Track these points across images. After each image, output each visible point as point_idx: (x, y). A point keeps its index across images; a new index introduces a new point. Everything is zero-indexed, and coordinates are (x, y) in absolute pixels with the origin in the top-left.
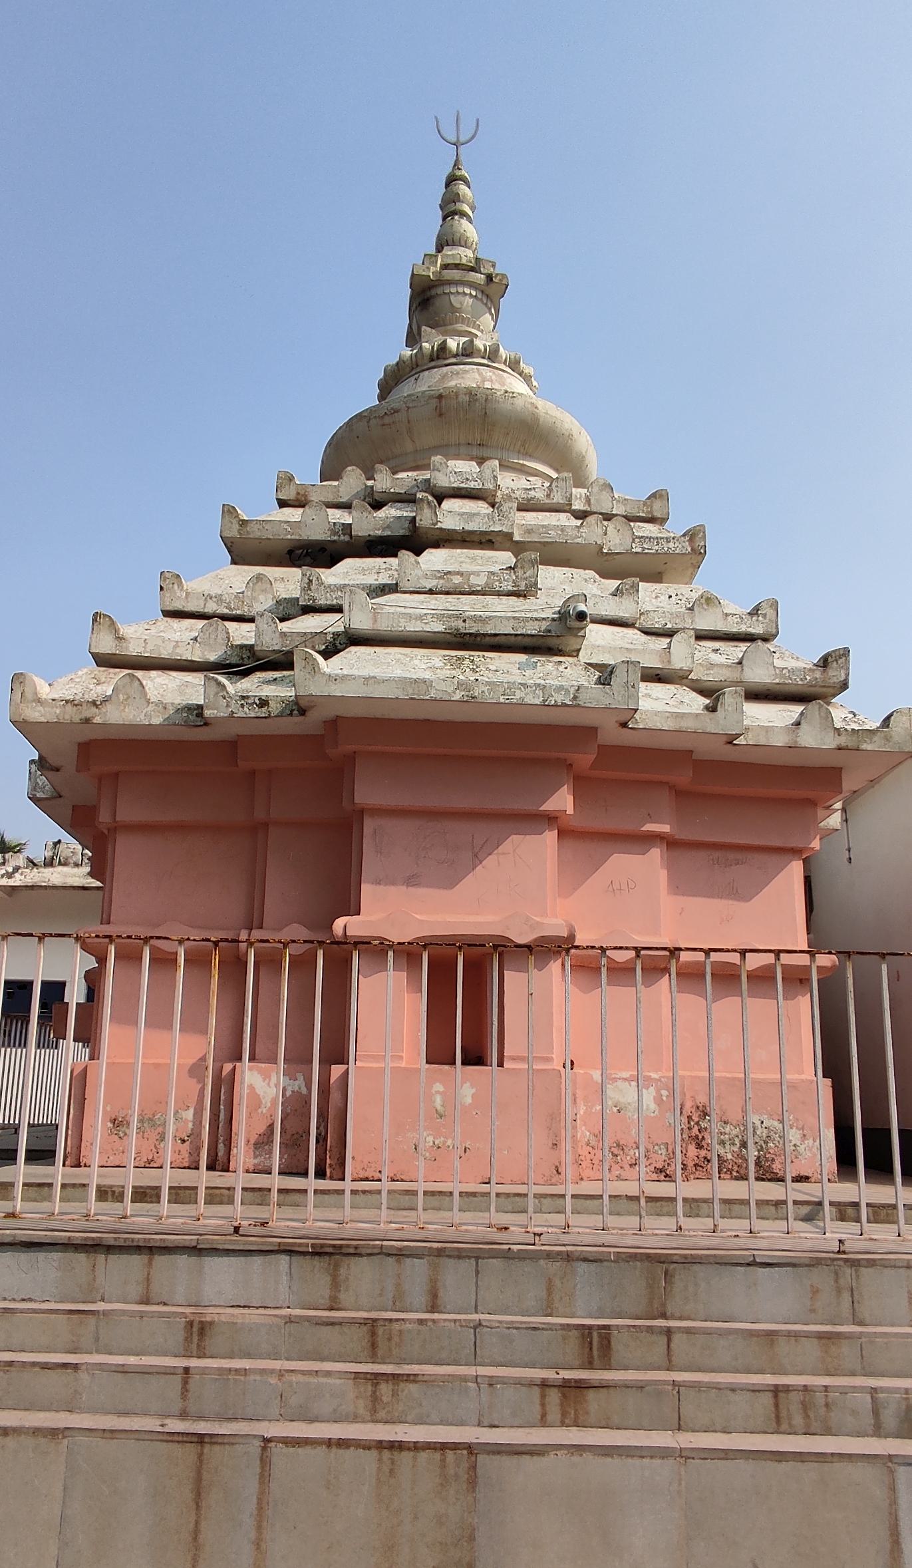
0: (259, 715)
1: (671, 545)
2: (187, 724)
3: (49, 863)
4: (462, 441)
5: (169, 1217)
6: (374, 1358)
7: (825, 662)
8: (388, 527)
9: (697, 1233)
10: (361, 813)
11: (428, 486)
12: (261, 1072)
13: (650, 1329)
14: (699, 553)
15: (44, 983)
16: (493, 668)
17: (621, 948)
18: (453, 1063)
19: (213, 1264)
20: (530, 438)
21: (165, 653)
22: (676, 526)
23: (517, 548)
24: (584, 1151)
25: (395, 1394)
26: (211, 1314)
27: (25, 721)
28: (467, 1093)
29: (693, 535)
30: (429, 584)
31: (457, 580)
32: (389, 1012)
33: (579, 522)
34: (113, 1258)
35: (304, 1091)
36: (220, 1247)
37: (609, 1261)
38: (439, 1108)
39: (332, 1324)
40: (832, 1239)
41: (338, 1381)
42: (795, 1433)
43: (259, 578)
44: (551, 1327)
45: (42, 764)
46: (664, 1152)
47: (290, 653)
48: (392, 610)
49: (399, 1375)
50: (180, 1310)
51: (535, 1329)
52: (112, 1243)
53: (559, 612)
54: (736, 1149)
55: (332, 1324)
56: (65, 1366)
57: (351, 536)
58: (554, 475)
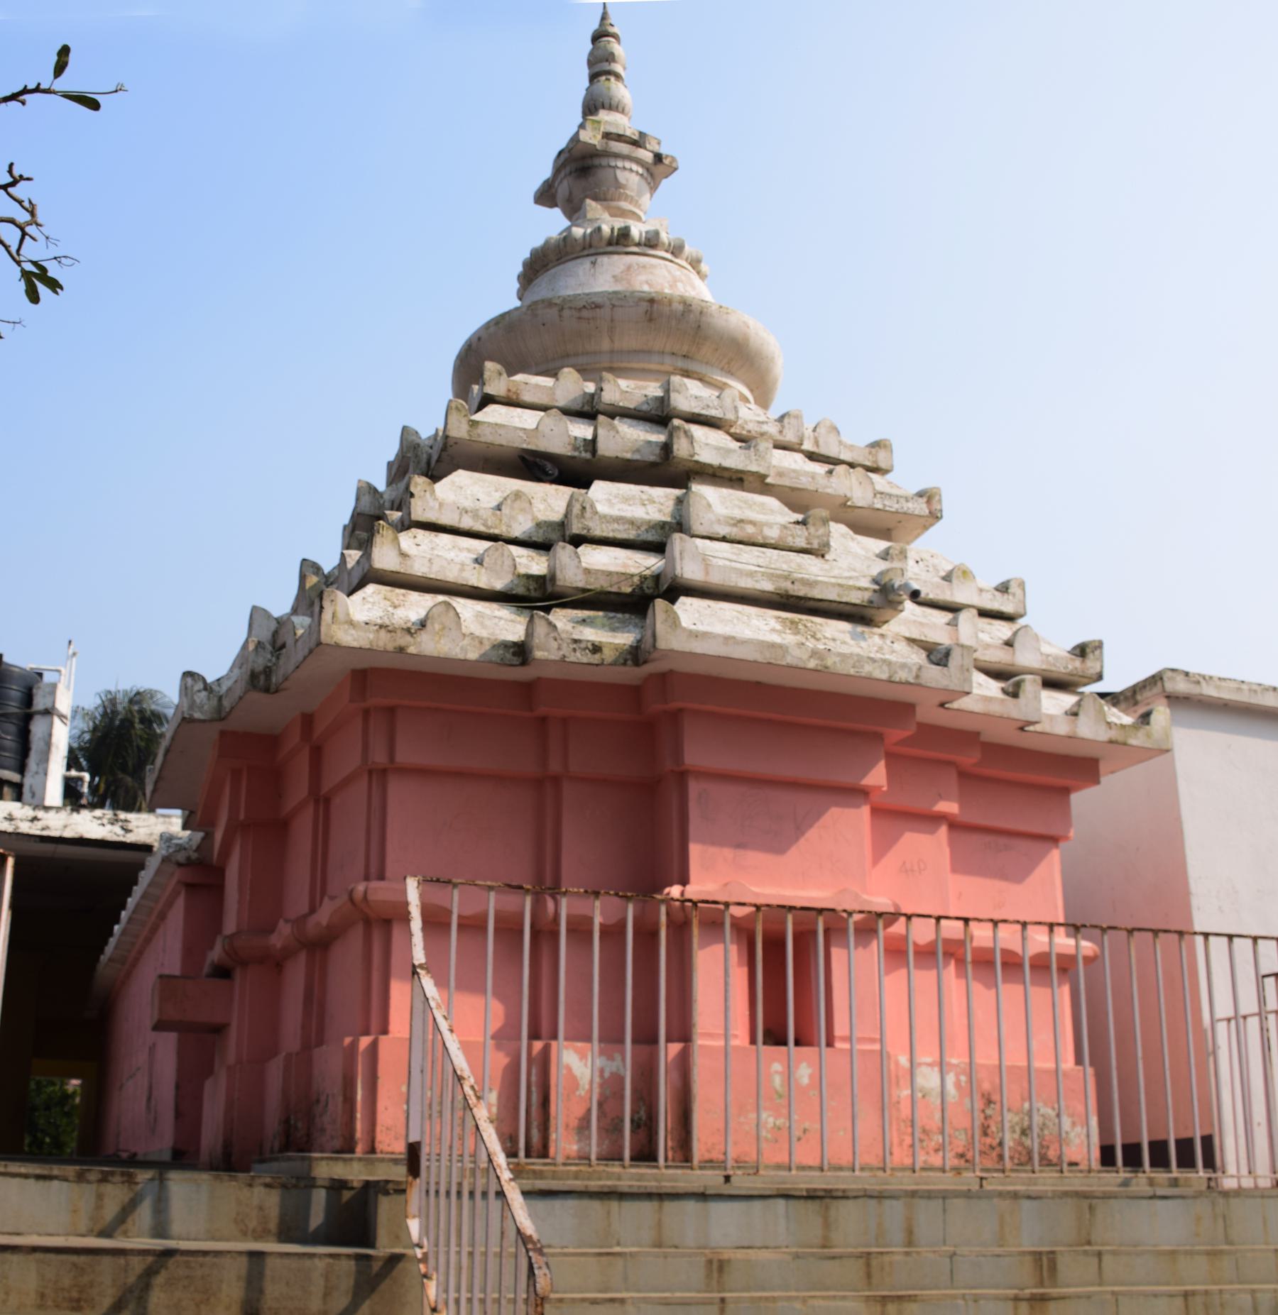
2: (503, 663)
4: (668, 349)
7: (1082, 651)
8: (638, 451)
12: (577, 1051)
18: (785, 1043)
19: (717, 1207)
26: (726, 1255)
28: (804, 1073)
29: (928, 495)
30: (723, 530)
31: (750, 530)
32: (719, 983)
37: (1047, 1198)
43: (518, 495)
46: (963, 1137)
53: (875, 581)
54: (1016, 1136)
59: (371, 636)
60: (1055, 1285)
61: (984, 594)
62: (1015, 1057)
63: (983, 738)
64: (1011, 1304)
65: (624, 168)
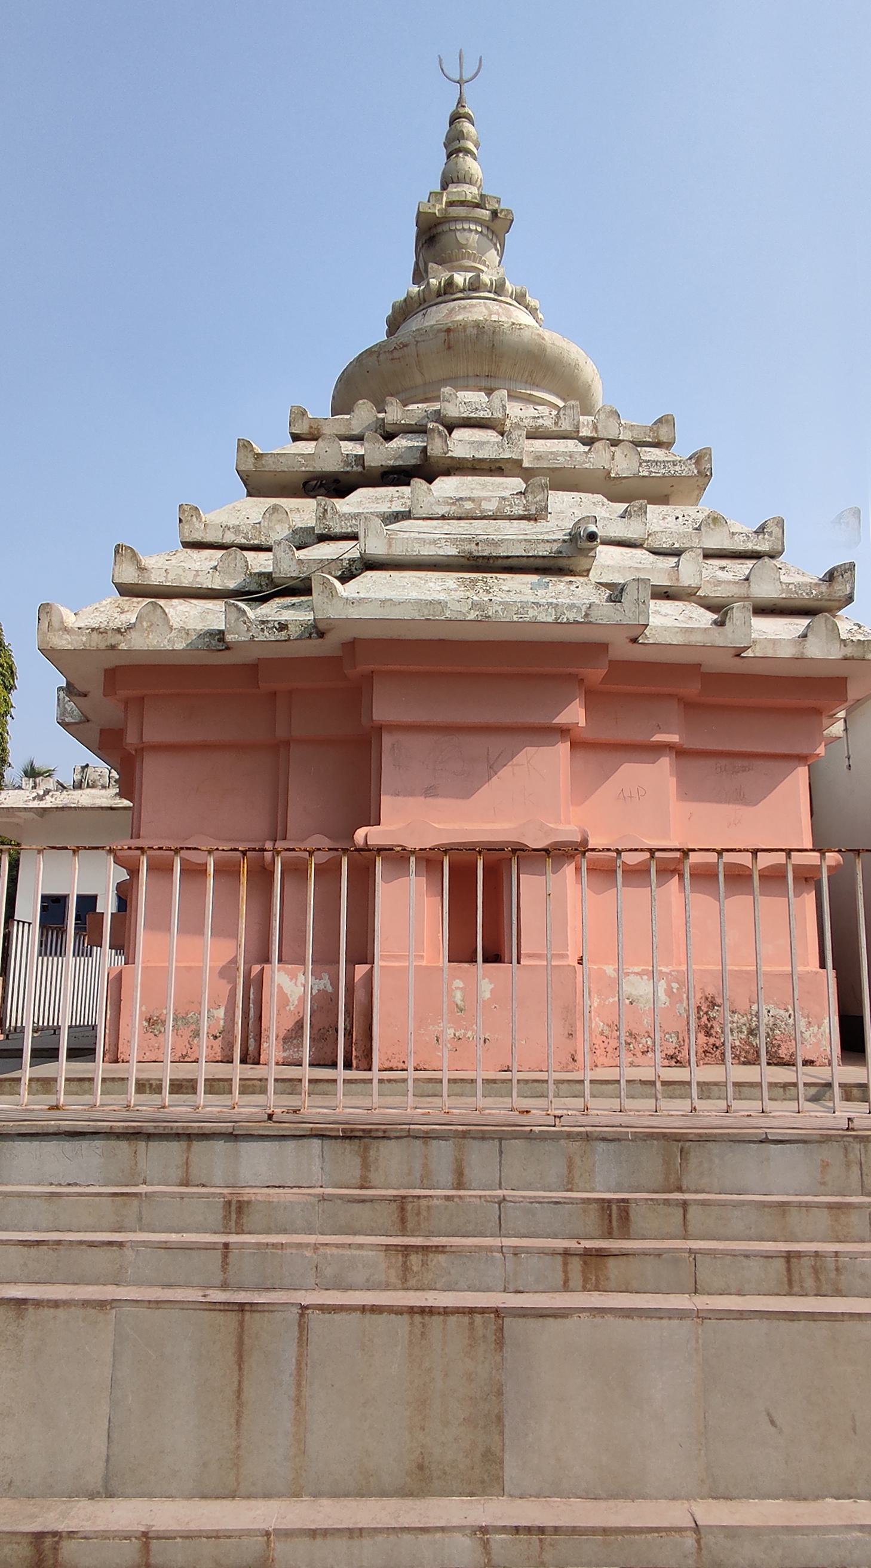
0: (278, 638)
1: (677, 468)
3: (78, 786)
5: (206, 1107)
6: (404, 1232)
7: (831, 577)
8: (400, 457)
9: (710, 1113)
10: (379, 729)
11: (438, 416)
12: (287, 972)
13: (667, 1202)
14: (705, 476)
15: (79, 897)
16: (506, 588)
17: (636, 850)
18: (473, 960)
20: (538, 369)
21: (187, 581)
22: (682, 450)
23: (527, 474)
24: (598, 1041)
25: (424, 1263)
26: (247, 1194)
27: (53, 649)
28: (486, 989)
29: (700, 458)
31: (469, 505)
32: (410, 916)
33: (587, 448)
34: (153, 1145)
35: (330, 989)
36: (255, 1133)
37: (627, 1140)
38: (459, 1002)
39: (363, 1201)
40: (841, 1117)
41: (370, 1253)
42: (806, 1295)
43: (275, 509)
44: (572, 1202)
45: (70, 690)
47: (308, 579)
48: (406, 535)
49: (427, 1247)
50: (218, 1190)
51: (557, 1203)
52: (152, 1131)
53: (570, 534)
55: (363, 1201)
56: (110, 1243)
57: (364, 467)
58: (561, 404)
59: (84, 639)
60: (626, 1236)
61: (736, 537)
62: (740, 962)
63: (703, 669)
64: (559, 1259)
65: (464, 230)
